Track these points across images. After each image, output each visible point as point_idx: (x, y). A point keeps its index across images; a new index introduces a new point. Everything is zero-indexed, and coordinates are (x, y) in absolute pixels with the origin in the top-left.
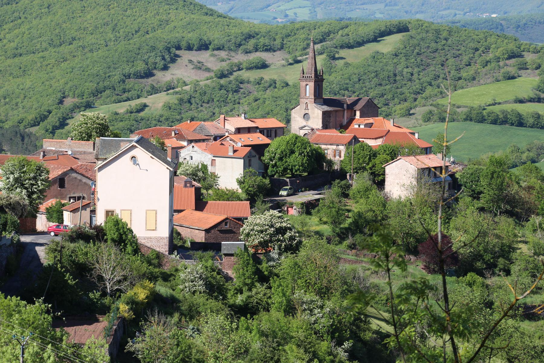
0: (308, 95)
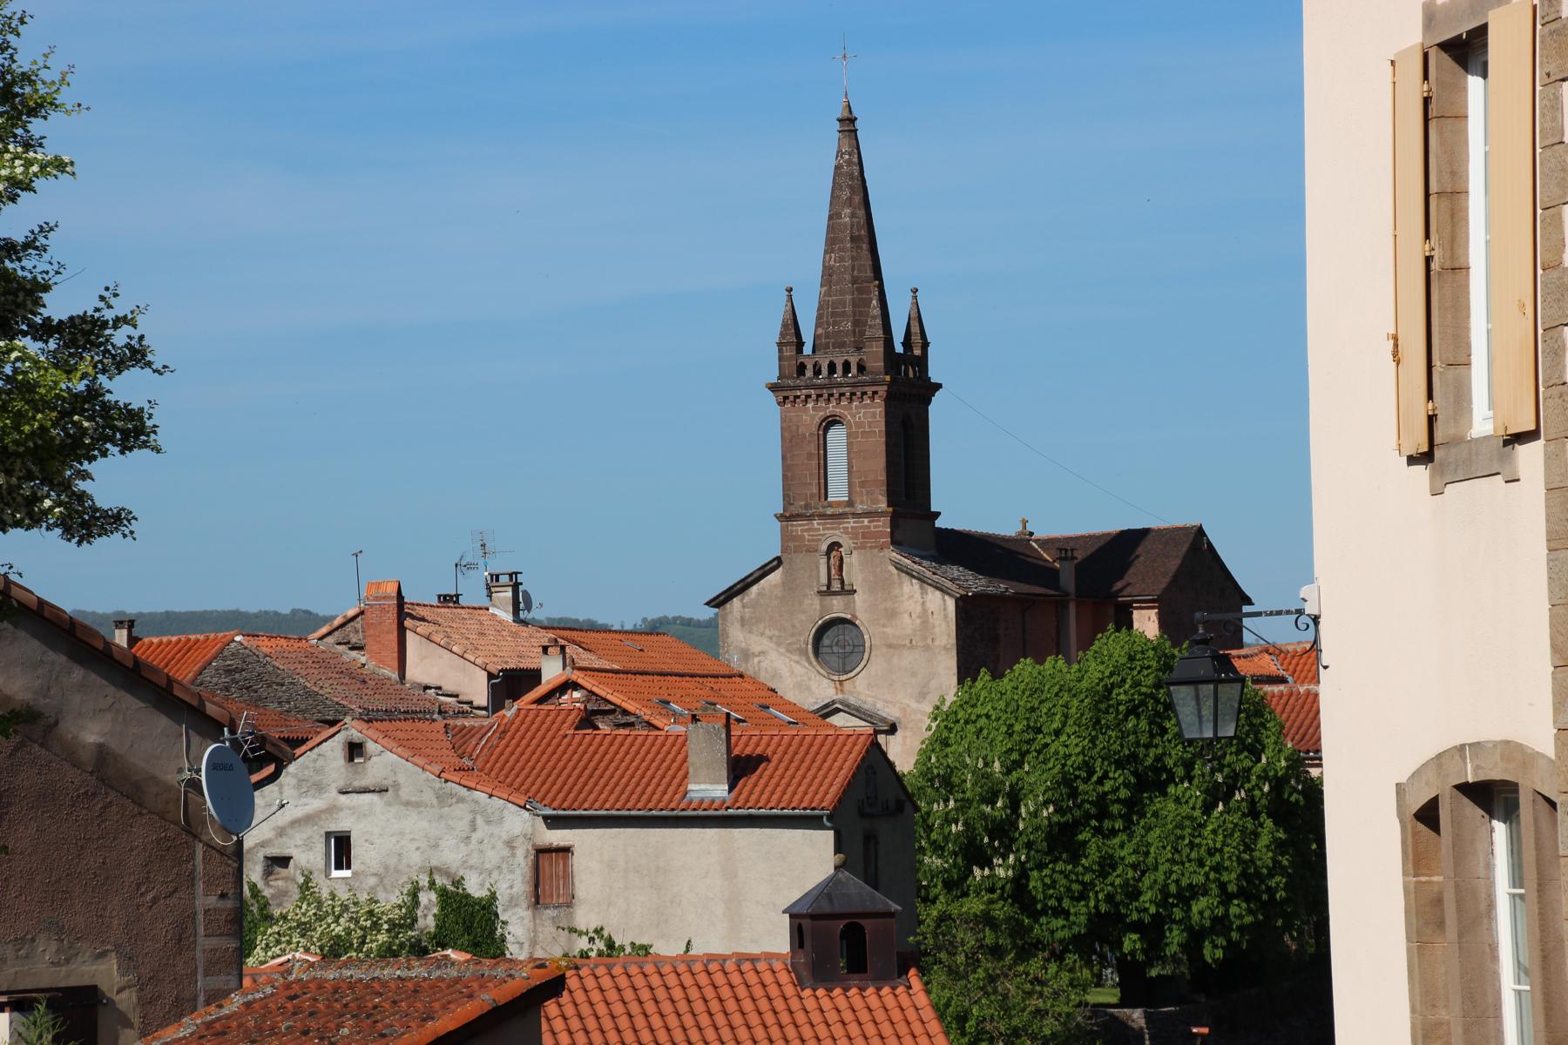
0: (838, 490)
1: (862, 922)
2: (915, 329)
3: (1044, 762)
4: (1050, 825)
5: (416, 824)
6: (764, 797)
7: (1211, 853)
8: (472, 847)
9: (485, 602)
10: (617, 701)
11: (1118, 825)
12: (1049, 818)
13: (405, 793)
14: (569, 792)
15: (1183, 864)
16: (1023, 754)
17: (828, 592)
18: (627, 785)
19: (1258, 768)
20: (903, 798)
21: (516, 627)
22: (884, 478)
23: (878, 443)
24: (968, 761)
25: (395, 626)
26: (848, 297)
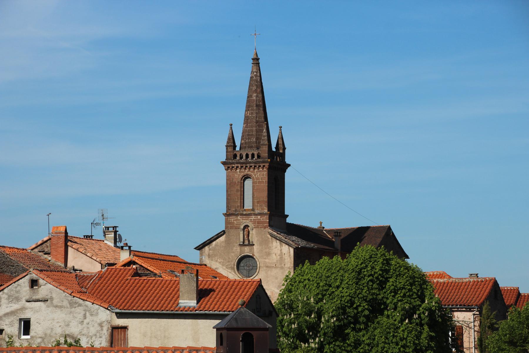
0: (248, 204)
1: (252, 332)
2: (280, 142)
3: (332, 299)
4: (334, 326)
5: (60, 315)
6: (212, 306)
7: (402, 339)
8: (84, 326)
9: (102, 238)
10: (152, 270)
11: (362, 326)
12: (334, 323)
13: (55, 302)
14: (128, 303)
15: (389, 344)
16: (324, 296)
17: (243, 245)
18: (153, 300)
19: (423, 306)
20: (272, 310)
21: (115, 248)
22: (267, 200)
23: (265, 186)
24: (300, 298)
25: (64, 245)
26: (254, 128)
